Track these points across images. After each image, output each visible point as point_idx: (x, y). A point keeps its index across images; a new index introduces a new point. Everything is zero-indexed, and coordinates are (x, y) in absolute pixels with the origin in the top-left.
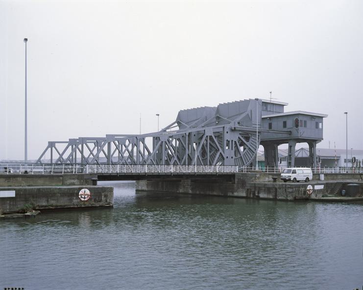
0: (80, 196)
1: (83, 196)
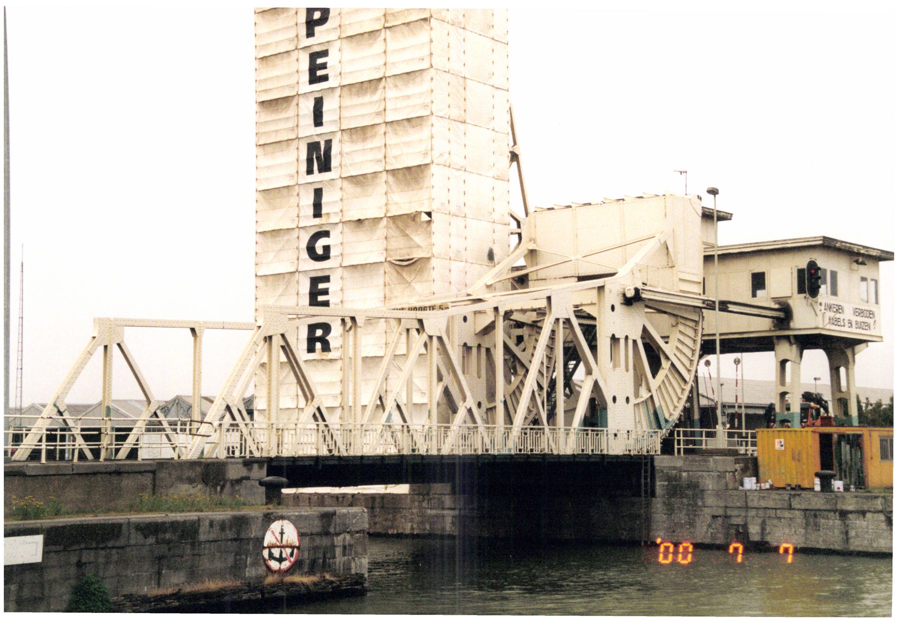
0: (266, 553)
1: (276, 552)
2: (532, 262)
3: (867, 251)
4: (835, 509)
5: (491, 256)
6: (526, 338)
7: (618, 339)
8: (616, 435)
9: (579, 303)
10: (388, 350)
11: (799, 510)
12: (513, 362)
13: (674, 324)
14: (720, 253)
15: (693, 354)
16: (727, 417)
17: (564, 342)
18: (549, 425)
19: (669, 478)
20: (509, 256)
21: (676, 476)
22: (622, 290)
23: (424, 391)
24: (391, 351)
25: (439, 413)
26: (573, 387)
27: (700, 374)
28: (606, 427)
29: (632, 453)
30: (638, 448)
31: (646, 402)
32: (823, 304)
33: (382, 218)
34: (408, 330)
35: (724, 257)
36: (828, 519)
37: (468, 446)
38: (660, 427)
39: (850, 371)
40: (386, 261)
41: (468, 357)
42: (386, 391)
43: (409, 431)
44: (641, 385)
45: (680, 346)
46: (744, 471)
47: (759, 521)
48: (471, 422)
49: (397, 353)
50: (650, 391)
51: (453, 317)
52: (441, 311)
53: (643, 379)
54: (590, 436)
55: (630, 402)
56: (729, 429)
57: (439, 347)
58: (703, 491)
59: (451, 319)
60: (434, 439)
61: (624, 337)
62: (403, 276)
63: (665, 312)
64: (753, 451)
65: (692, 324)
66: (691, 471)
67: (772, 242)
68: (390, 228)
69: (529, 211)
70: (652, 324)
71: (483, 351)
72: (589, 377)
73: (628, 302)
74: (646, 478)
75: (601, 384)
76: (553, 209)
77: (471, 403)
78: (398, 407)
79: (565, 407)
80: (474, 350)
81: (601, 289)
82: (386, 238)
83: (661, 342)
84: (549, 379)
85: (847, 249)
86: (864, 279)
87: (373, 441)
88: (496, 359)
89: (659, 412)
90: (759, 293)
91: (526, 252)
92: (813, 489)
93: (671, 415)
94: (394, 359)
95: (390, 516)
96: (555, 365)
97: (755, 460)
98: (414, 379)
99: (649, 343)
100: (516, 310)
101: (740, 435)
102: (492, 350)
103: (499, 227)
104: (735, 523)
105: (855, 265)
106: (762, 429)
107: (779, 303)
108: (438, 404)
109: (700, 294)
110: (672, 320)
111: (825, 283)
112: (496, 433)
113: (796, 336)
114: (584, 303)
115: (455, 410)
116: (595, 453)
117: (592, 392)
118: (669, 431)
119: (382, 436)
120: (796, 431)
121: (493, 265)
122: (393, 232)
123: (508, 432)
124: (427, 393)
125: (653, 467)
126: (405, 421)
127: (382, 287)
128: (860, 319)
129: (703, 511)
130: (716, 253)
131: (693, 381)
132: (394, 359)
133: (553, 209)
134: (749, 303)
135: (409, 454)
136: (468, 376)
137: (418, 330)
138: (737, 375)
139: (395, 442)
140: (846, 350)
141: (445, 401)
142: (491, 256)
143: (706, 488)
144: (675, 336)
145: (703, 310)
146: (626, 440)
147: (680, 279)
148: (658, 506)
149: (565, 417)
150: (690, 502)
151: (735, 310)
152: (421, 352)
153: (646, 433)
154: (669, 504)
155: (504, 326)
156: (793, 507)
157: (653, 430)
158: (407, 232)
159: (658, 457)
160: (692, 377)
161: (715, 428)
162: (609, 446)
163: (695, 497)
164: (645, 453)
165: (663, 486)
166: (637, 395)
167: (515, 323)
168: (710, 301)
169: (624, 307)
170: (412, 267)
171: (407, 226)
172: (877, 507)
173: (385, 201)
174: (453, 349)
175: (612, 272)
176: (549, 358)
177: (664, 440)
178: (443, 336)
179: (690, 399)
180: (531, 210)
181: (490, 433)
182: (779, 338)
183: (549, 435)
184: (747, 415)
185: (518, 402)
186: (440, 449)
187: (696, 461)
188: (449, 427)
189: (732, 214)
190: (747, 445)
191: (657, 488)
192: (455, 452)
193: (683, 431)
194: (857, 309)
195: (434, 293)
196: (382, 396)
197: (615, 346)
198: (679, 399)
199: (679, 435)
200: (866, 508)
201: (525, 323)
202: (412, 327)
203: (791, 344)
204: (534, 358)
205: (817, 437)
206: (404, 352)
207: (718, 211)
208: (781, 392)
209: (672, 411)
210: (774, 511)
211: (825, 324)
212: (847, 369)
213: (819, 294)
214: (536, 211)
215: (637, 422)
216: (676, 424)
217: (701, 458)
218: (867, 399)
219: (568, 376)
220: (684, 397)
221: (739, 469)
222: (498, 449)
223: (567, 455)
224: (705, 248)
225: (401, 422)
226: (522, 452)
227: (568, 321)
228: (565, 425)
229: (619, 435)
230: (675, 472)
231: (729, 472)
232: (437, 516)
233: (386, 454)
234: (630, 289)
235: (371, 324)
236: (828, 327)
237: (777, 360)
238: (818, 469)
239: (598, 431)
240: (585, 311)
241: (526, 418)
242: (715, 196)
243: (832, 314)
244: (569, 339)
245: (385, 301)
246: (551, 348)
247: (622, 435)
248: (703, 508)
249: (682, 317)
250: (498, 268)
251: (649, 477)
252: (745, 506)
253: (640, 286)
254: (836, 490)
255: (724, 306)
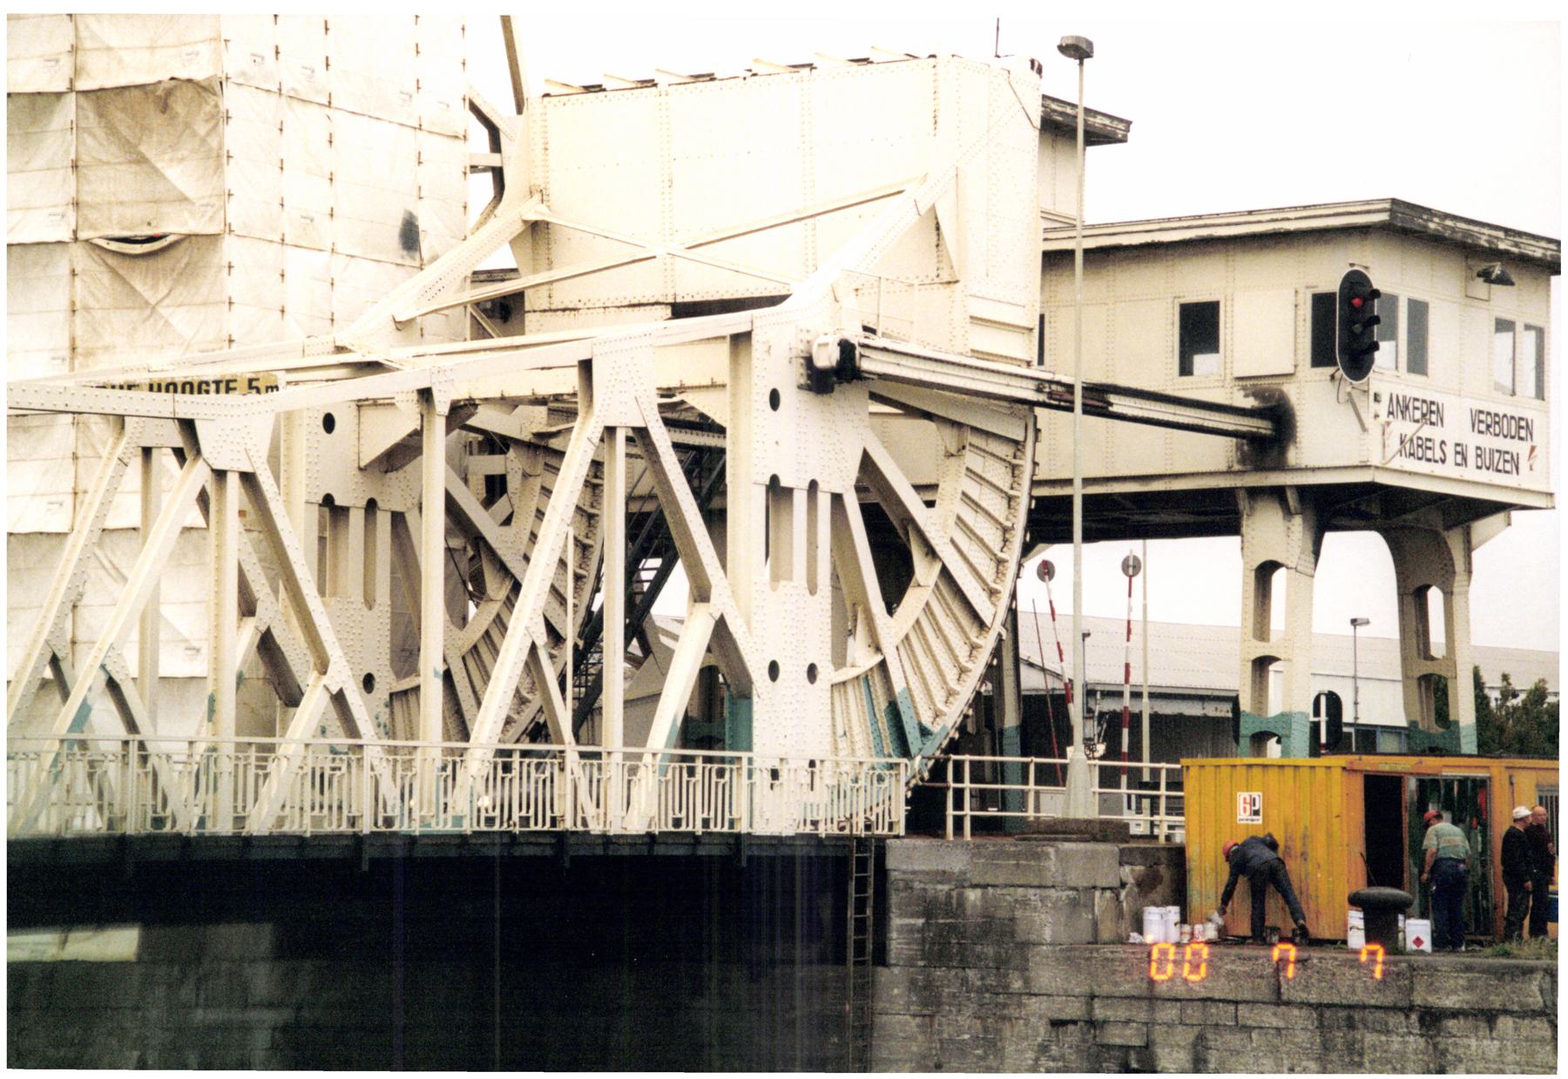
2: (535, 260)
3: (1516, 245)
4: (1404, 1003)
5: (410, 237)
6: (513, 483)
7: (789, 492)
8: (775, 774)
9: (674, 383)
10: (81, 512)
11: (1303, 1005)
12: (472, 559)
13: (953, 450)
14: (1092, 244)
15: (1005, 541)
16: (1100, 724)
17: (630, 499)
18: (578, 741)
19: (929, 909)
20: (465, 239)
21: (948, 903)
22: (802, 347)
23: (196, 644)
24: (92, 515)
25: (241, 704)
26: (651, 640)
27: (1023, 606)
28: (749, 748)
29: (822, 831)
30: (840, 814)
31: (866, 678)
32: (1385, 399)
33: (59, 95)
34: (147, 452)
35: (1103, 257)
36: (1388, 1032)
37: (330, 807)
38: (905, 751)
39: (1457, 601)
40: (76, 239)
41: (335, 539)
42: (74, 642)
43: (144, 759)
44: (852, 633)
45: (969, 516)
46: (1146, 886)
47: (1191, 1036)
48: (341, 731)
49: (110, 524)
50: (878, 649)
51: (289, 415)
52: (253, 396)
53: (860, 617)
54: (699, 776)
55: (819, 677)
56: (1102, 758)
57: (248, 507)
58: (1025, 945)
59: (287, 419)
60: (226, 784)
61: (806, 485)
62: (132, 288)
63: (928, 416)
64: (1171, 827)
65: (1005, 451)
66: (994, 886)
67: (1241, 214)
68: (87, 130)
69: (525, 96)
70: (886, 444)
71: (383, 521)
72: (701, 606)
73: (820, 381)
74: (861, 905)
75: (736, 627)
76: (599, 88)
77: (342, 676)
78: (113, 686)
79: (626, 691)
80: (357, 518)
81: (740, 340)
82: (75, 166)
83: (913, 503)
84: (582, 612)
85: (1459, 236)
86: (1503, 325)
87: (27, 795)
88: (423, 551)
89: (902, 708)
90: (1201, 361)
91: (519, 228)
92: (1345, 942)
93: (937, 715)
94: (100, 544)
95: (73, 1032)
96: (599, 570)
97: (1178, 855)
98: (165, 610)
99: (877, 505)
100: (486, 400)
101: (1135, 780)
102: (411, 518)
103: (434, 147)
104: (1118, 1041)
105: (1480, 288)
106: (1200, 760)
107: (1257, 394)
108: (240, 679)
109: (1029, 364)
110: (949, 438)
111: (1392, 336)
112: (417, 763)
113: (1302, 490)
114: (688, 383)
115: (292, 698)
116: (712, 829)
117: (709, 650)
118: (931, 763)
119: (57, 776)
120: (1296, 767)
121: (417, 264)
122: (96, 147)
123: (454, 763)
124: (204, 651)
125: (882, 872)
126: (132, 726)
127: (62, 316)
128: (1488, 442)
129: (1025, 1005)
130: (1079, 245)
131: (1004, 625)
132: (100, 544)
133: (599, 88)
134: (1170, 392)
135: (143, 832)
136: (332, 601)
137: (179, 453)
138: (1130, 609)
139: (101, 795)
140: (1445, 534)
141: (261, 671)
142: (410, 237)
143: (1033, 937)
144: (953, 485)
145: (1038, 411)
146: (806, 788)
147: (972, 317)
148: (896, 991)
149: (626, 719)
150: (988, 982)
151: (1130, 412)
152: (188, 524)
153: (865, 767)
154: (928, 986)
155: (447, 446)
156: (1285, 997)
157: (884, 760)
158: (143, 148)
159: (898, 841)
160: (1002, 613)
161: (1063, 755)
162: (756, 813)
163: (1001, 964)
164: (860, 831)
165: (911, 929)
166: (839, 659)
167: (480, 438)
168: (1059, 383)
169: (808, 396)
170: (160, 263)
171: (143, 128)
172: (1531, 1000)
173: (70, 39)
174: (289, 512)
175: (775, 293)
176: (584, 548)
177: (916, 790)
178: (258, 473)
179: (993, 673)
180: (531, 91)
181: (399, 767)
182: (1255, 493)
183: (578, 772)
184: (1156, 718)
185: (486, 677)
186: (244, 818)
187: (1009, 856)
188: (271, 748)
189: (1128, 123)
190: (1154, 810)
191: (894, 935)
192: (291, 828)
193: (972, 763)
194: (1481, 412)
195: (231, 341)
196: (60, 655)
197: (777, 511)
198: (963, 671)
199: (958, 777)
200: (1496, 1002)
201: (511, 439)
202: (159, 442)
203: (1288, 513)
204: (537, 547)
205: (1358, 784)
206: (136, 521)
207: (1088, 111)
208: (1253, 657)
209: (941, 706)
210: (1232, 1008)
211: (1389, 456)
212: (1448, 594)
213: (1374, 367)
214: (547, 95)
215: (838, 735)
216: (952, 740)
217: (1022, 847)
218: (1505, 678)
219: (638, 607)
220: (978, 667)
221: (1131, 880)
222: (422, 818)
223: (632, 837)
224: (1046, 230)
225: (121, 732)
226: (496, 828)
227: (640, 436)
228: (626, 744)
229: (783, 775)
230: (946, 887)
231: (1104, 889)
232: (225, 1027)
233: (69, 835)
234: (826, 345)
235: (26, 430)
236: (1398, 463)
237: (1246, 563)
238: (1361, 886)
239: (722, 760)
240: (692, 408)
241: (509, 721)
242: (1081, 64)
243: (1408, 428)
244: (642, 489)
245: (72, 359)
246: (588, 517)
247: (794, 775)
248: (1025, 1000)
249: (975, 430)
250: (431, 272)
251: (871, 902)
252: (1145, 993)
253: (856, 336)
254: (1411, 946)
255: (1098, 399)
